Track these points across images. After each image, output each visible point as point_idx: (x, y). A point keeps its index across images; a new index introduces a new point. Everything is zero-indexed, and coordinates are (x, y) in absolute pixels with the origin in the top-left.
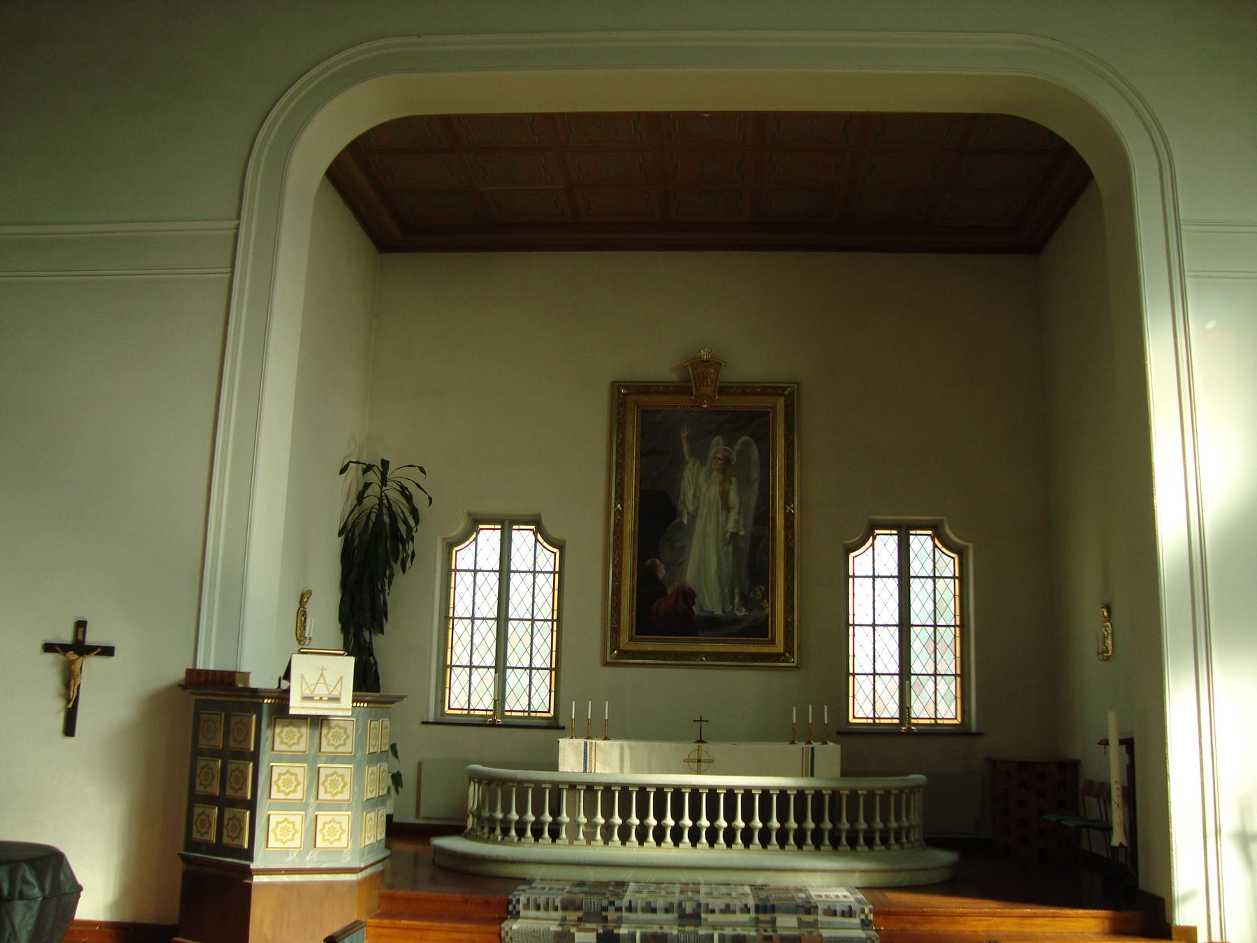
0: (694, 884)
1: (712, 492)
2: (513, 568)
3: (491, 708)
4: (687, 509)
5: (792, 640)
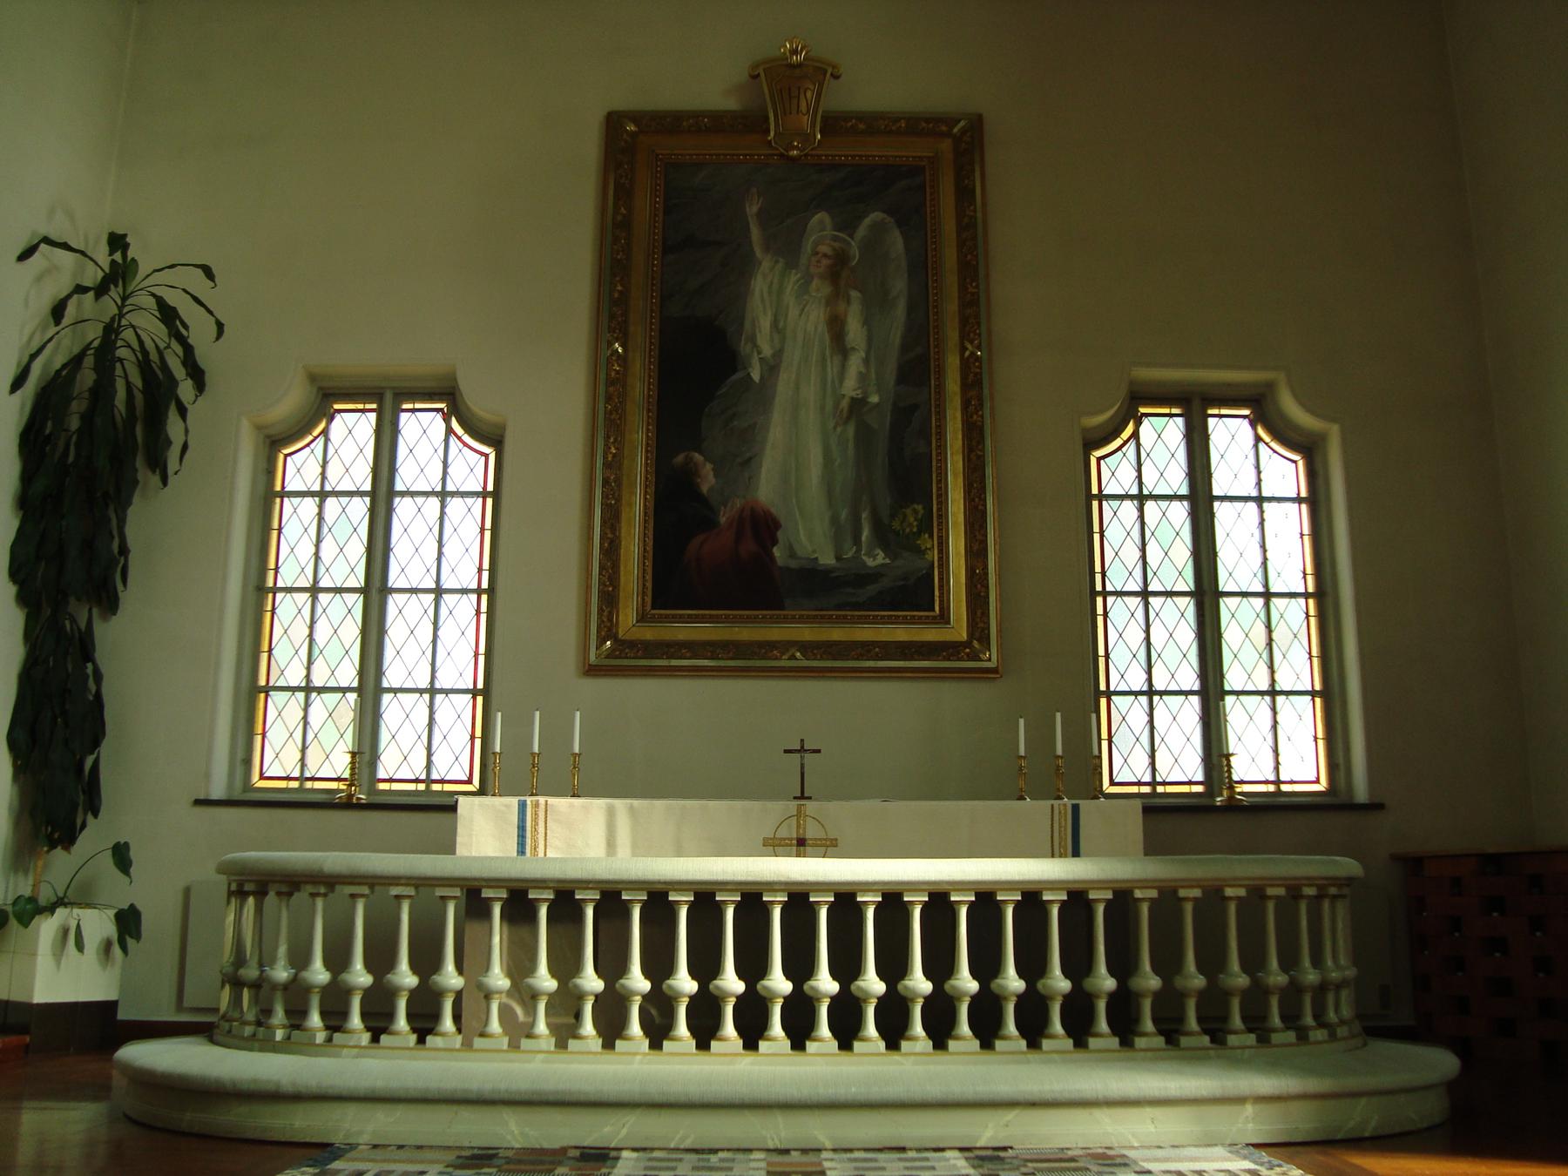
0: (805, 1151)
1: (809, 320)
2: (399, 487)
3: (347, 775)
4: (759, 353)
5: (986, 614)
